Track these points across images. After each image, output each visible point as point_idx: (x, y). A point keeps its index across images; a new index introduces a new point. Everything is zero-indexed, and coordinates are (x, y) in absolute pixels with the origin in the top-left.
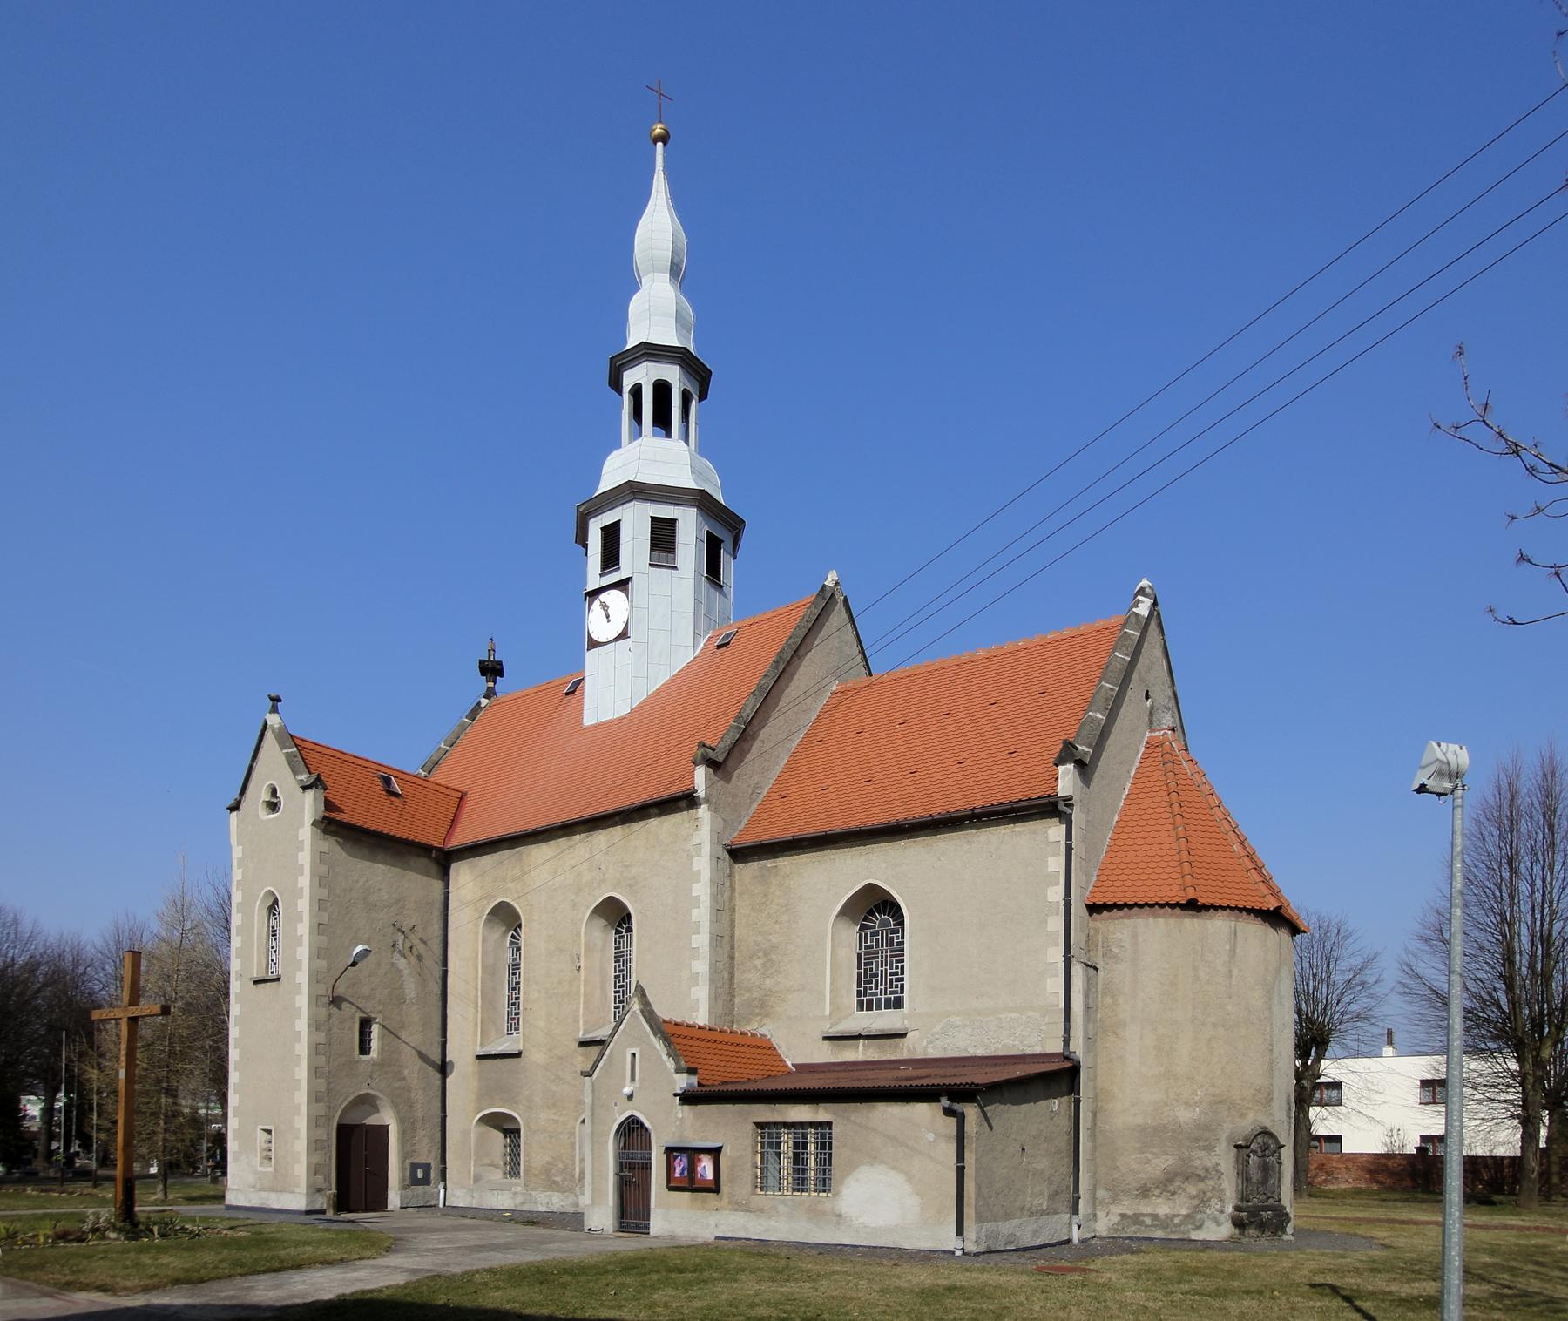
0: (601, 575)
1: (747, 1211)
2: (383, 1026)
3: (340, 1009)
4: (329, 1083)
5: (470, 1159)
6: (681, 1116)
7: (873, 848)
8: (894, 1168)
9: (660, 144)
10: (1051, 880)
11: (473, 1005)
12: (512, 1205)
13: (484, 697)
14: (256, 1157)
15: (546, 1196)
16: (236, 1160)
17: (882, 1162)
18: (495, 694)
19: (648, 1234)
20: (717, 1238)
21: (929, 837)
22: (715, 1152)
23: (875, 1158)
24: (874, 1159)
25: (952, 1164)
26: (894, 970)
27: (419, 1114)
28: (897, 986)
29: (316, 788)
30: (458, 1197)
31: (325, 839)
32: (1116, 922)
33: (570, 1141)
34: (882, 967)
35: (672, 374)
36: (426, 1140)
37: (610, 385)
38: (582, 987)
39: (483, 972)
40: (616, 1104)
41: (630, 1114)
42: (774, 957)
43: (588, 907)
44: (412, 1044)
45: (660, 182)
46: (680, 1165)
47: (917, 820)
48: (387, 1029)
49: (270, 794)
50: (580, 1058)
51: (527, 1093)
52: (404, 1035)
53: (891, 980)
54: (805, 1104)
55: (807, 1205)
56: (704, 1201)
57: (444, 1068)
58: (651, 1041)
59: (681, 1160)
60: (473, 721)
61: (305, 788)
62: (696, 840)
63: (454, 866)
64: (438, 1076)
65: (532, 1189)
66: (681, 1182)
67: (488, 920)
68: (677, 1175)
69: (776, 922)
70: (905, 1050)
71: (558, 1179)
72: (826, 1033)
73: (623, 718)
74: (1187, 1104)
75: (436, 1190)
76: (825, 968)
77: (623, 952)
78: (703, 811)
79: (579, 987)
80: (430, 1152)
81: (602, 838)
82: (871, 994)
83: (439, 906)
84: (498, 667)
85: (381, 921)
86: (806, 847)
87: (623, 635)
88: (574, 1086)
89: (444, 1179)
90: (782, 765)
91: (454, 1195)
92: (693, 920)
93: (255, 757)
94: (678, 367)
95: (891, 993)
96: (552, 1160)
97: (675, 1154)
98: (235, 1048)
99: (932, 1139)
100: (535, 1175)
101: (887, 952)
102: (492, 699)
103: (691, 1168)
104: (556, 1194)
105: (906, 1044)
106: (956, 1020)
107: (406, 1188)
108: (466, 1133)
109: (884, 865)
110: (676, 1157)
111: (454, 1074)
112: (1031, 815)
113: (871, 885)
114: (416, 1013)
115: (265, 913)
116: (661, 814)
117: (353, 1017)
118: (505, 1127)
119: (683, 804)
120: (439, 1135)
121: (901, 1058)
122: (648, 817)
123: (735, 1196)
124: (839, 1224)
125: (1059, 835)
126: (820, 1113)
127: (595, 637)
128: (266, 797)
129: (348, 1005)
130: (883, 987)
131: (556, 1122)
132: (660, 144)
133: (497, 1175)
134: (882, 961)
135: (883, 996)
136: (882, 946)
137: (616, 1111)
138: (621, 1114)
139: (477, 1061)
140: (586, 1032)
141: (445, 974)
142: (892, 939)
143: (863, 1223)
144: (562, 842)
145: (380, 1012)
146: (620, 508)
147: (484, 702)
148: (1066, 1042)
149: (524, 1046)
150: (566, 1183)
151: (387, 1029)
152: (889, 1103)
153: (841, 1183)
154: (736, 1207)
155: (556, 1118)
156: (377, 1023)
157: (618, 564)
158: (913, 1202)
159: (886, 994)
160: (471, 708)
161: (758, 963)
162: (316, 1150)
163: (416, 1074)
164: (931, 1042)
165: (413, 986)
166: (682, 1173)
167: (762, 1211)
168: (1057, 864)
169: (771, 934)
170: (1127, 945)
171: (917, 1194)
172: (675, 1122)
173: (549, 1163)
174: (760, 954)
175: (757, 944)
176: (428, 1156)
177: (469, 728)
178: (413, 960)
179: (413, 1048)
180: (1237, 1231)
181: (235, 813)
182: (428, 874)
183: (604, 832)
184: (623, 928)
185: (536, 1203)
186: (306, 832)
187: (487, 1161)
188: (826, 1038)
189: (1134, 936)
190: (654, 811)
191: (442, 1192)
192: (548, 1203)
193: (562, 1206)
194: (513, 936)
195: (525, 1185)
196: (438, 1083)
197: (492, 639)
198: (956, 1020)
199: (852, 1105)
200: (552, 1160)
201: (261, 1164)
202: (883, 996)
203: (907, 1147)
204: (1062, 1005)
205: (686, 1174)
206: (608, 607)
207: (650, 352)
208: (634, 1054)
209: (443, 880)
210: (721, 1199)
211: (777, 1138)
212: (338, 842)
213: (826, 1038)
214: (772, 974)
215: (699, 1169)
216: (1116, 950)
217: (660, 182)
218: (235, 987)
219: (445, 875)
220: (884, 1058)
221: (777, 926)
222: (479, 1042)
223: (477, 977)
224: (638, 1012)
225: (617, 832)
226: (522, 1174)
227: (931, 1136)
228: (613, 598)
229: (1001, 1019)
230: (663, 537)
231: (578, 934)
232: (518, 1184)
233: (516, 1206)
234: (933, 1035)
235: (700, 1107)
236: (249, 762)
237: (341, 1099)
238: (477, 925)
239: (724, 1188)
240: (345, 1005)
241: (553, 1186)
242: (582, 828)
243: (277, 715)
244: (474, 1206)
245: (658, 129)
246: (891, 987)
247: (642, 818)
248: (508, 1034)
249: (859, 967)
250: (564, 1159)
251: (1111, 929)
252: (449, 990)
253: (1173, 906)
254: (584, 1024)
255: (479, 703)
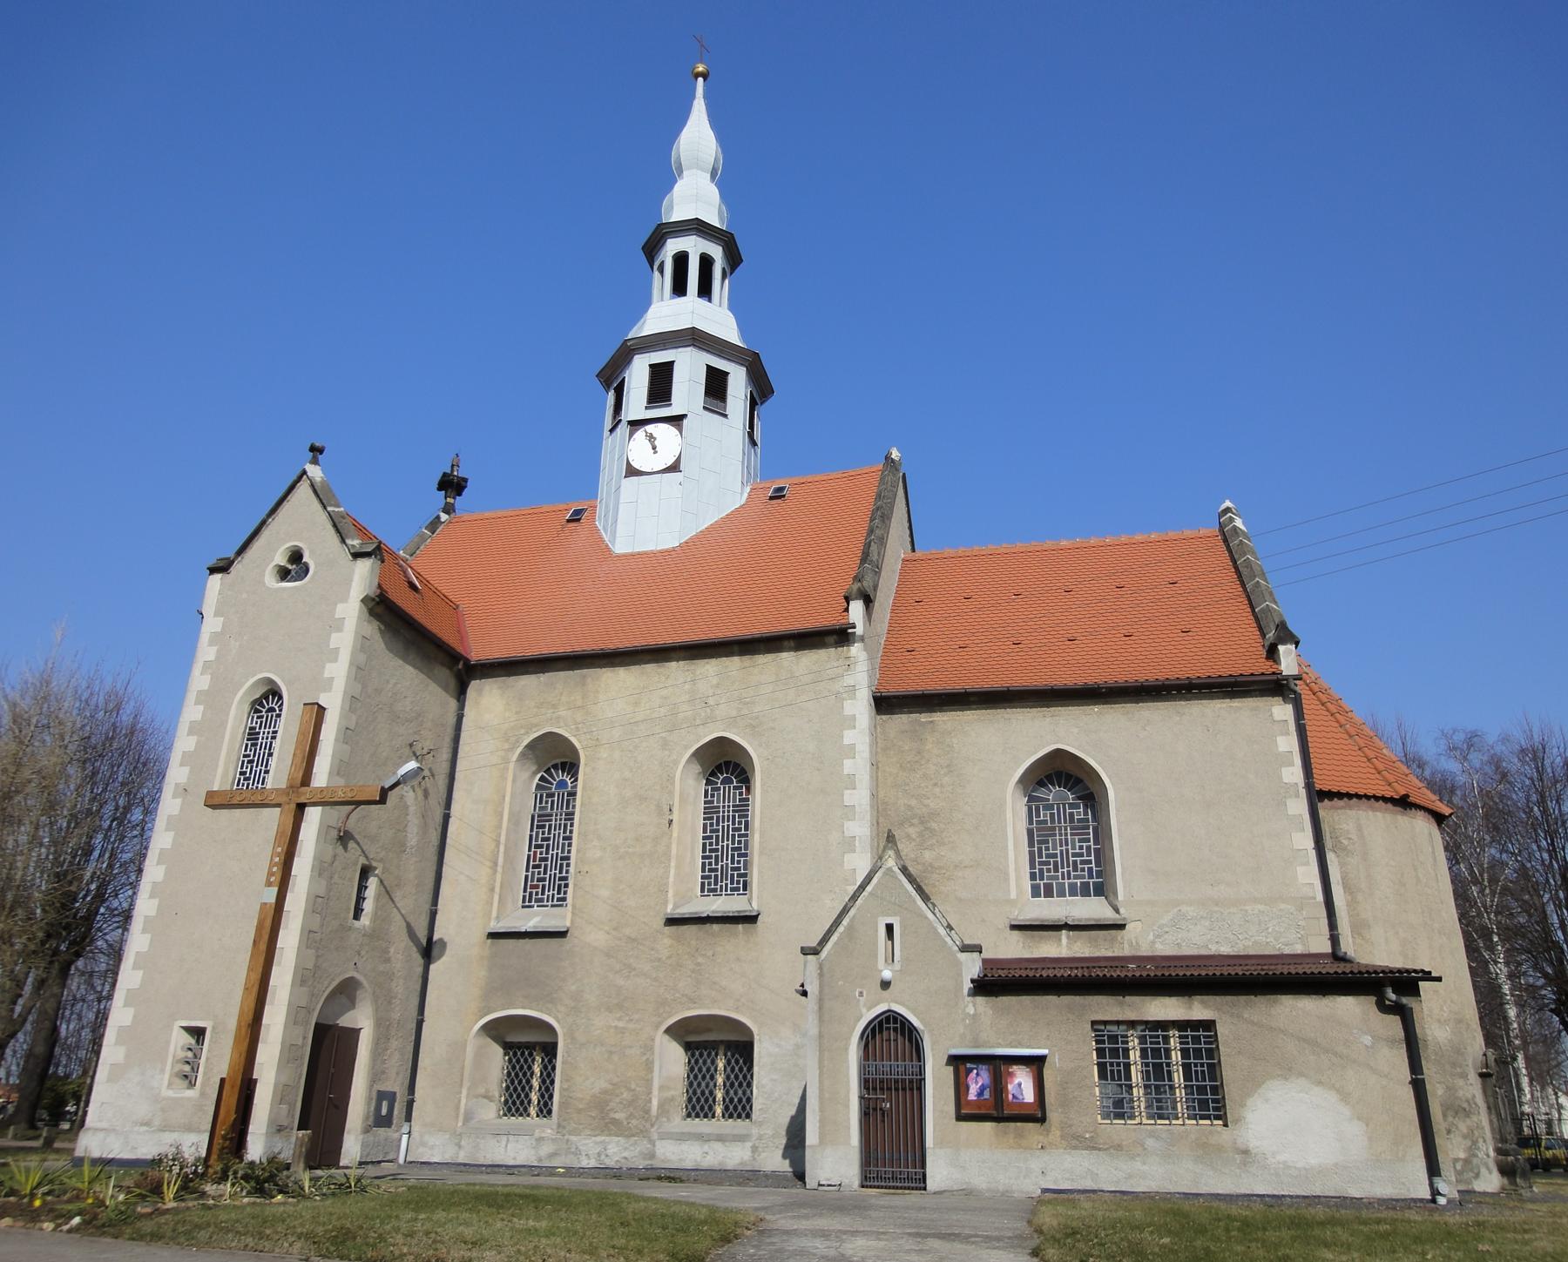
0: (646, 407)
1: (1094, 1148)
2: (381, 881)
3: (345, 848)
4: (318, 957)
5: (461, 1085)
6: (972, 1012)
7: (1060, 711)
8: (1320, 1083)
9: (700, 80)
10: (1286, 760)
11: (488, 864)
12: (533, 1158)
13: (443, 512)
14: (163, 1071)
15: (596, 1143)
16: (117, 1072)
17: (1301, 1075)
18: (455, 511)
19: (925, 1189)
20: (1045, 1191)
21: (1129, 705)
22: (1036, 1063)
23: (1290, 1069)
24: (1287, 1070)
25: (743, 1123)
26: (735, 885)
27: (396, 1016)
28: (1083, 870)
29: (375, 557)
30: (432, 1148)
31: (369, 622)
32: (1339, 811)
33: (644, 1058)
34: (1061, 846)
35: (716, 252)
36: (397, 1056)
37: (643, 248)
38: (674, 847)
39: (509, 820)
40: (861, 994)
41: (886, 1009)
42: (934, 825)
43: (686, 747)
44: (403, 912)
45: (699, 109)
46: (977, 1082)
47: (1173, 682)
48: (385, 887)
49: (287, 559)
50: (667, 941)
51: (573, 988)
52: (397, 896)
53: (1075, 863)
54: (1170, 996)
55: (1193, 1137)
56: (1020, 1135)
57: (429, 950)
58: (920, 909)
59: (978, 1074)
60: (433, 533)
61: (357, 555)
62: (848, 680)
63: (474, 685)
64: (418, 960)
65: (575, 1132)
66: (980, 1108)
67: (523, 755)
68: (972, 1096)
69: (936, 784)
70: (1126, 946)
71: (619, 1116)
72: (1015, 920)
73: (674, 549)
74: (1439, 1021)
75: (396, 1135)
76: (1007, 840)
77: (719, 807)
78: (856, 650)
79: (669, 846)
80: (397, 1074)
81: (709, 669)
82: (1049, 878)
83: (450, 731)
84: (463, 483)
85: (401, 738)
86: (974, 703)
87: (674, 468)
88: (656, 979)
89: (408, 1118)
90: (887, 621)
91: (423, 1144)
92: (846, 772)
93: (273, 511)
94: (721, 248)
95: (1076, 877)
96: (611, 1087)
97: (968, 1065)
98: (151, 897)
99: (1369, 1044)
100: (579, 1111)
101: (1066, 829)
102: (452, 515)
103: (998, 1085)
104: (616, 1139)
105: (1126, 938)
106: (1190, 911)
107: (368, 1132)
108: (458, 1048)
109: (1076, 730)
110: (969, 1071)
111: (444, 959)
112: (1251, 691)
113: (1058, 751)
114: (412, 867)
115: (247, 707)
116: (798, 648)
117: (355, 864)
118: (509, 1039)
119: (831, 639)
120: (410, 1048)
121: (1121, 955)
122: (780, 650)
123: (1071, 1126)
124: (1245, 1165)
125: (1285, 715)
126: (1198, 1009)
127: (636, 465)
128: (281, 559)
129: (355, 845)
130: (1065, 870)
131: (622, 1031)
132: (700, 80)
133: (490, 1112)
134: (1061, 840)
135: (1066, 881)
136: (1059, 822)
137: (862, 1003)
138: (869, 1009)
139: (489, 941)
140: (676, 906)
141: (446, 818)
142: (1071, 815)
143: (1285, 1162)
144: (650, 668)
145: (381, 860)
146: (674, 351)
147: (444, 517)
148: (1334, 940)
149: (572, 921)
150: (634, 1122)
151: (385, 887)
152: (1297, 996)
153: (1243, 1105)
154: (1074, 1142)
155: (621, 1024)
156: (376, 876)
157: (670, 400)
158: (1355, 1130)
159: (1069, 878)
160: (430, 520)
161: (912, 831)
162: (288, 1062)
163: (403, 954)
164: (1159, 936)
165: (415, 830)
166: (980, 1093)
167: (1119, 1147)
168: (1289, 743)
169: (929, 798)
170: (1354, 837)
171: (1359, 1119)
172: (963, 1020)
173: (605, 1092)
174: (915, 821)
175: (910, 808)
176: (396, 1085)
177: (429, 540)
178: (420, 793)
179: (403, 916)
180: (1505, 1181)
181: (218, 576)
182: (446, 689)
183: (713, 662)
184: (719, 778)
185: (577, 1153)
186: (351, 611)
187: (482, 1090)
188: (1014, 927)
189: (1360, 828)
190: (736, 648)
191: (405, 1137)
192: (599, 1154)
193: (626, 1158)
194: (542, 779)
195: (559, 1126)
196: (420, 970)
197: (457, 455)
198: (1190, 911)
199: (1242, 999)
200: (611, 1087)
201: (170, 1085)
202: (1066, 881)
203: (1336, 1054)
204: (1320, 897)
205: (987, 1095)
206: (655, 439)
207: (698, 227)
208: (890, 928)
209: (458, 701)
210: (1048, 1131)
211: (1123, 1042)
212: (380, 629)
213: (1014, 927)
214: (932, 845)
215: (1010, 1087)
216: (1345, 842)
217: (699, 109)
218: (169, 805)
219: (461, 693)
220: (1097, 954)
221: (937, 790)
222: (494, 914)
223: (499, 826)
224: (896, 869)
225: (734, 664)
226: (555, 1108)
227: (1367, 1040)
228: (663, 431)
229: (1246, 911)
230: (716, 385)
231: (671, 779)
232: (546, 1128)
233: (540, 1160)
234: (1161, 927)
235: (1001, 999)
236: (263, 516)
237: (326, 983)
238: (506, 761)
239: (1053, 1115)
240: (351, 845)
241: (609, 1126)
242: (682, 654)
243: (318, 467)
244: (460, 1160)
245: (701, 68)
246: (1075, 869)
247: (656, 661)
248: (523, 907)
249: (1031, 844)
250: (633, 1086)
251: (1336, 818)
252: (448, 840)
253: (1385, 799)
254: (674, 896)
255: (438, 517)
